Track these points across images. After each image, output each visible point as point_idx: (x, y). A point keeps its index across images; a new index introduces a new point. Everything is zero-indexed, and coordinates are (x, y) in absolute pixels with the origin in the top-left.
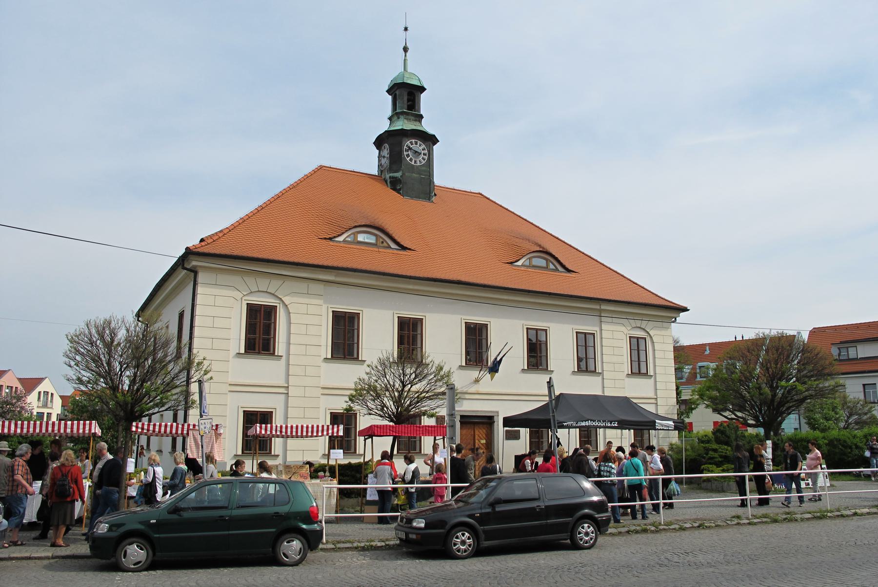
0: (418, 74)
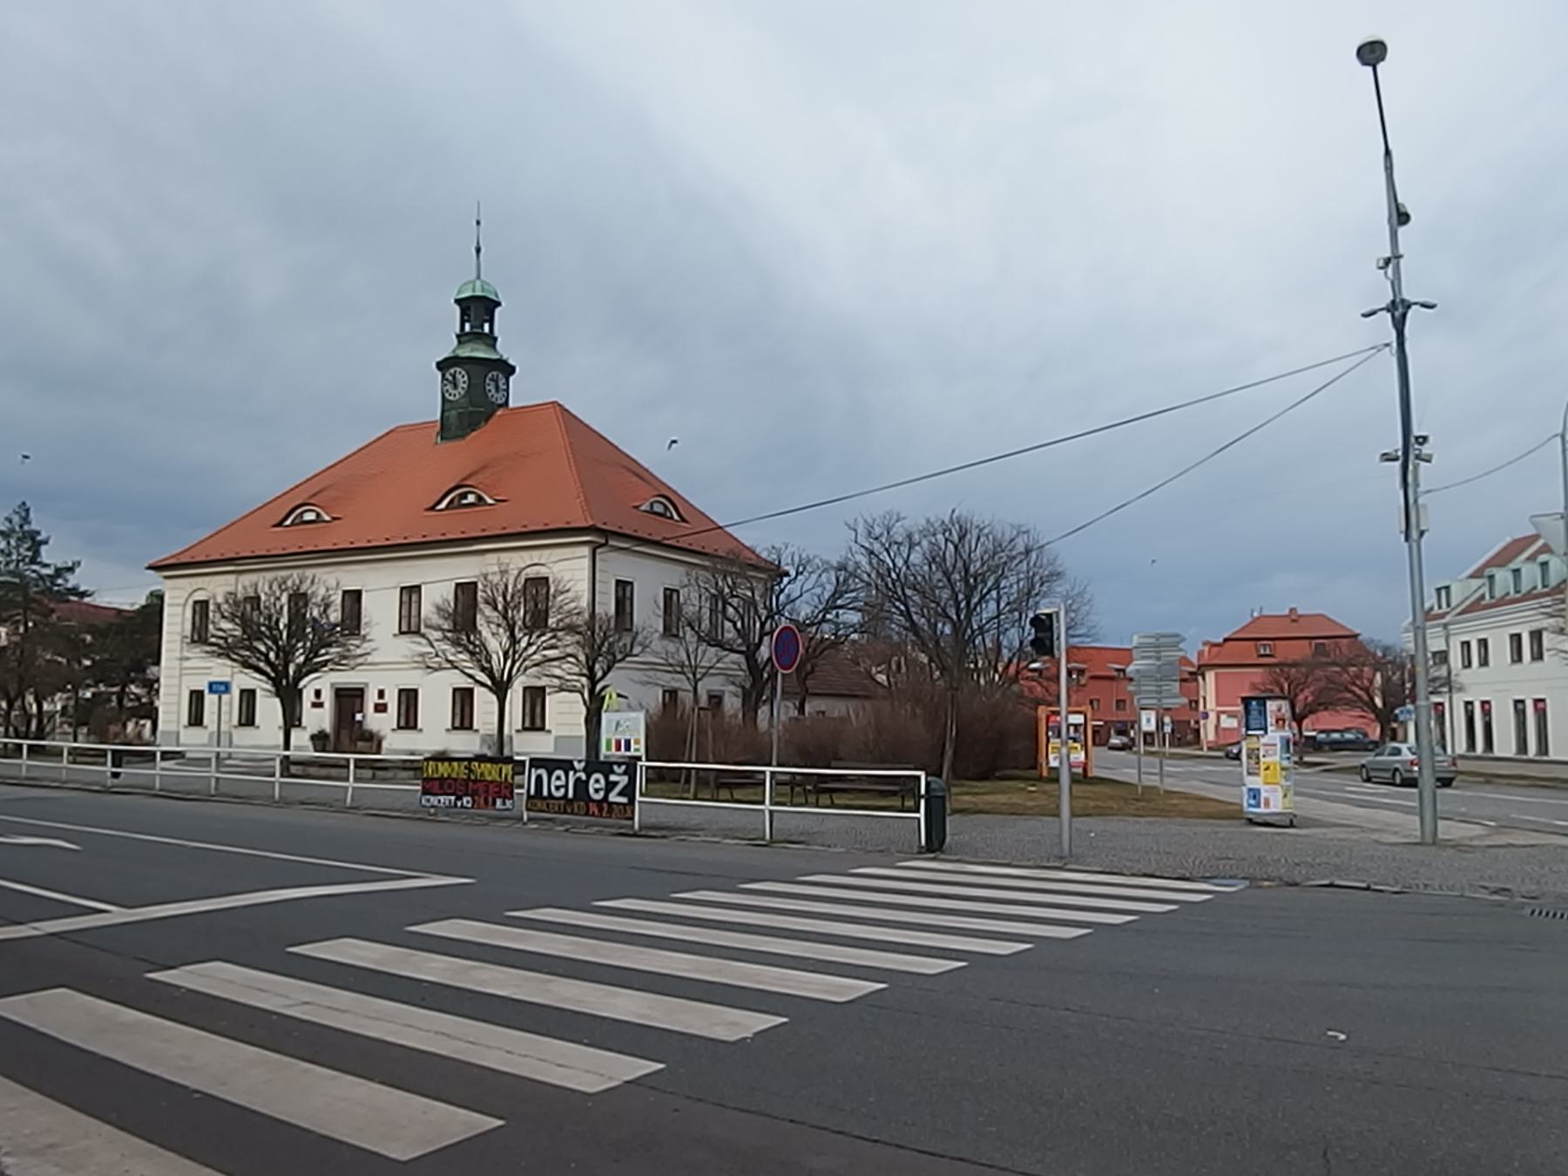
0: (496, 284)
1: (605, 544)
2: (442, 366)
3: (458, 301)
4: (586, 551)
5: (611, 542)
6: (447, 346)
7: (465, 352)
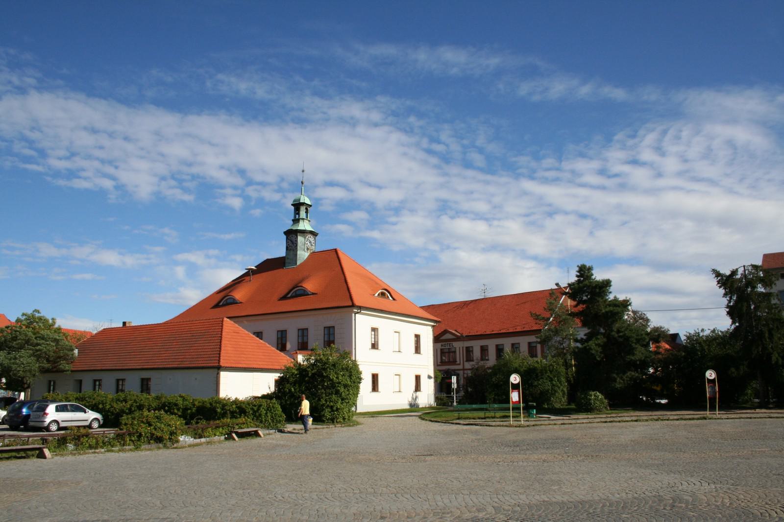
3: (292, 205)
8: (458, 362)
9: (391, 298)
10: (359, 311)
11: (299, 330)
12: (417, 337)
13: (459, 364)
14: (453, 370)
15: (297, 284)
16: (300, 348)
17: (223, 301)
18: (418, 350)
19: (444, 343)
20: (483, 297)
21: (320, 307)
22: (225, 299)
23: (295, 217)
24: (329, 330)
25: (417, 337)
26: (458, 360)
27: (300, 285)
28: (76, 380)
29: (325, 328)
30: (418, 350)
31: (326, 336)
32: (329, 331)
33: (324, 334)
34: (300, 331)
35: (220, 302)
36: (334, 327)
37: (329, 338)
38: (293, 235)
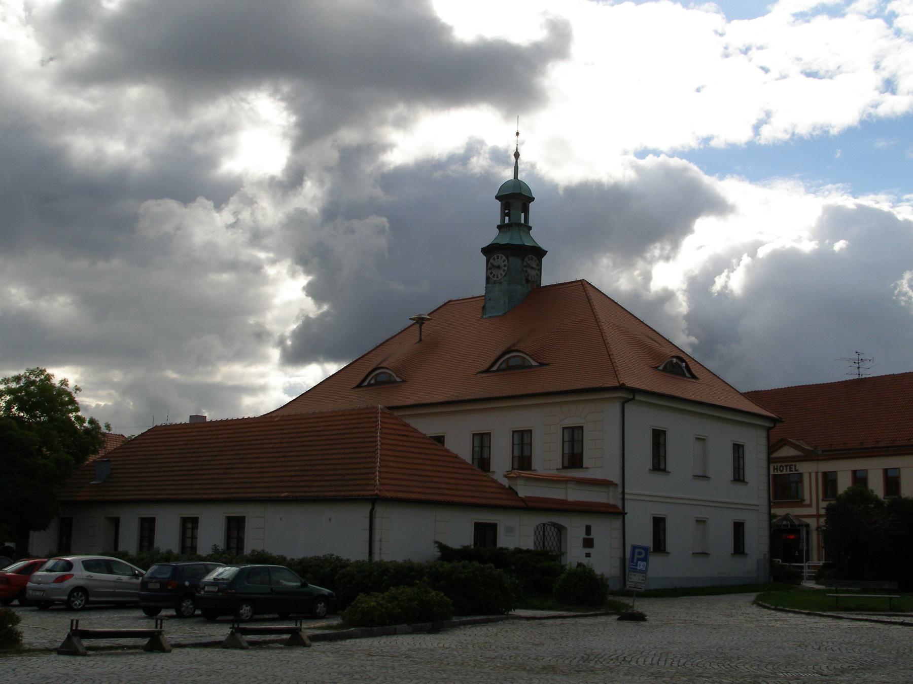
1: (634, 399)
2: (488, 251)
3: (497, 198)
4: (617, 407)
5: (637, 398)
6: (491, 236)
7: (505, 241)
8: (807, 502)
9: (687, 374)
10: (631, 397)
11: (514, 432)
12: (738, 449)
13: (810, 506)
14: (797, 516)
15: (514, 345)
16: (566, 464)
17: (500, 361)
18: (739, 477)
19: (779, 465)
20: (856, 377)
21: (577, 387)
22: (503, 359)
23: (503, 220)
24: (522, 435)
25: (738, 449)
26: (806, 496)
27: (516, 348)
28: (109, 518)
29: (564, 428)
30: (739, 477)
31: (566, 445)
32: (573, 435)
33: (563, 442)
34: (566, 432)
35: (364, 381)
36: (582, 428)
37: (573, 449)
38: (500, 255)
